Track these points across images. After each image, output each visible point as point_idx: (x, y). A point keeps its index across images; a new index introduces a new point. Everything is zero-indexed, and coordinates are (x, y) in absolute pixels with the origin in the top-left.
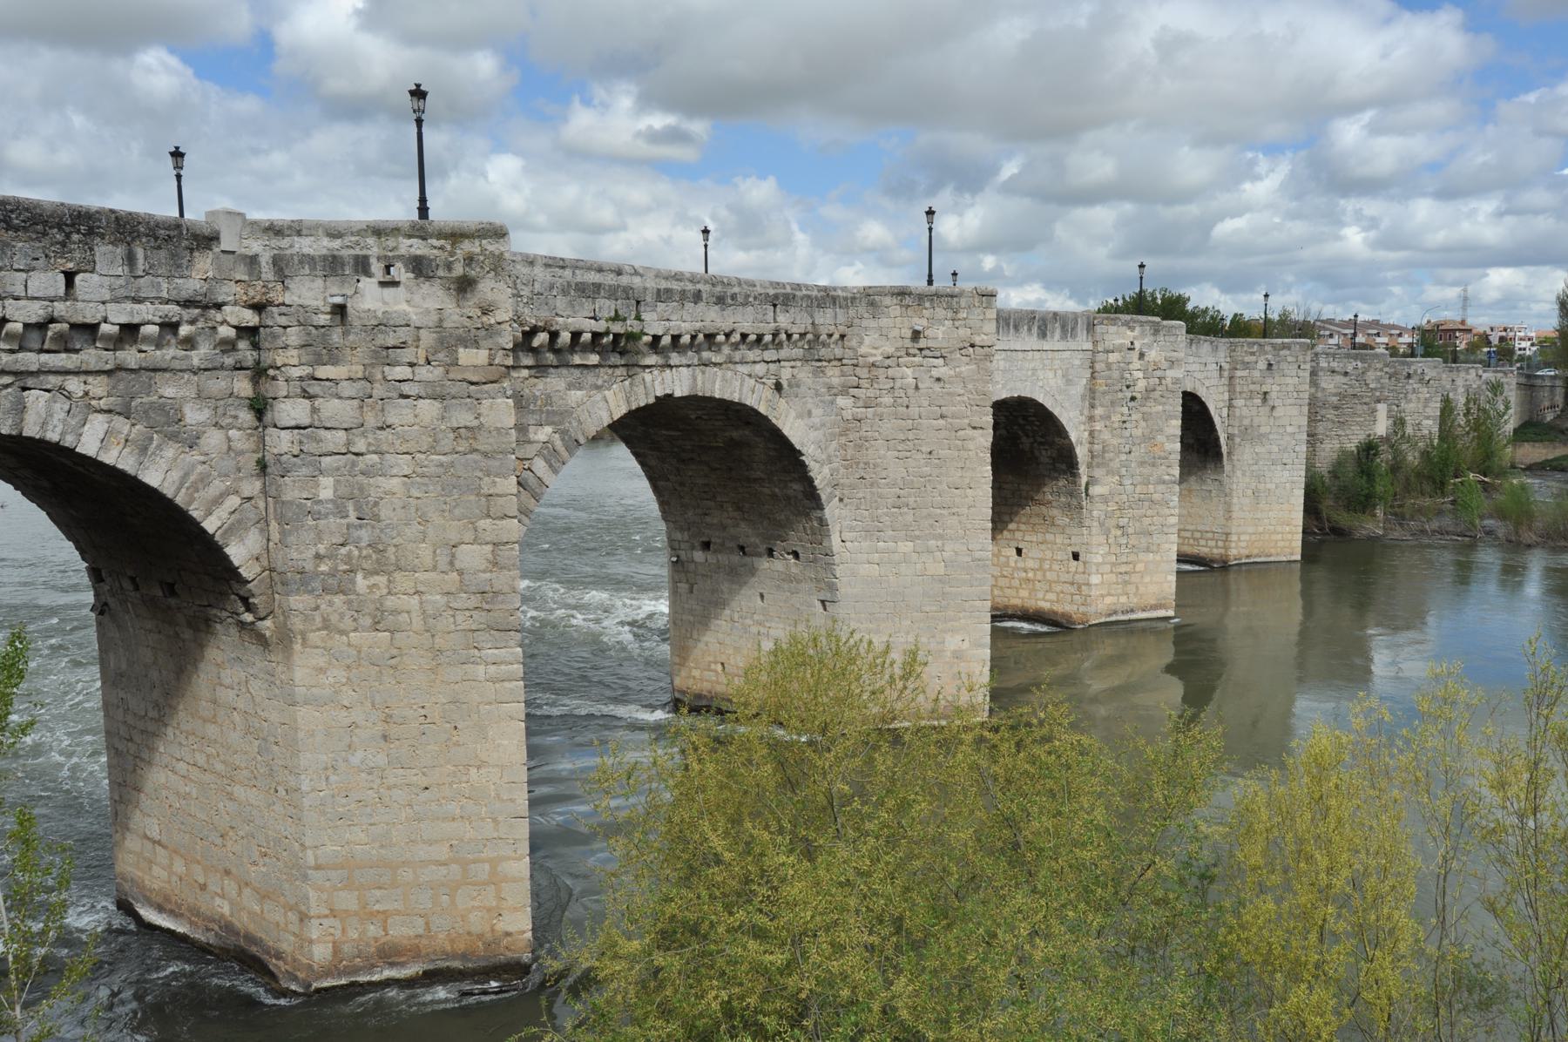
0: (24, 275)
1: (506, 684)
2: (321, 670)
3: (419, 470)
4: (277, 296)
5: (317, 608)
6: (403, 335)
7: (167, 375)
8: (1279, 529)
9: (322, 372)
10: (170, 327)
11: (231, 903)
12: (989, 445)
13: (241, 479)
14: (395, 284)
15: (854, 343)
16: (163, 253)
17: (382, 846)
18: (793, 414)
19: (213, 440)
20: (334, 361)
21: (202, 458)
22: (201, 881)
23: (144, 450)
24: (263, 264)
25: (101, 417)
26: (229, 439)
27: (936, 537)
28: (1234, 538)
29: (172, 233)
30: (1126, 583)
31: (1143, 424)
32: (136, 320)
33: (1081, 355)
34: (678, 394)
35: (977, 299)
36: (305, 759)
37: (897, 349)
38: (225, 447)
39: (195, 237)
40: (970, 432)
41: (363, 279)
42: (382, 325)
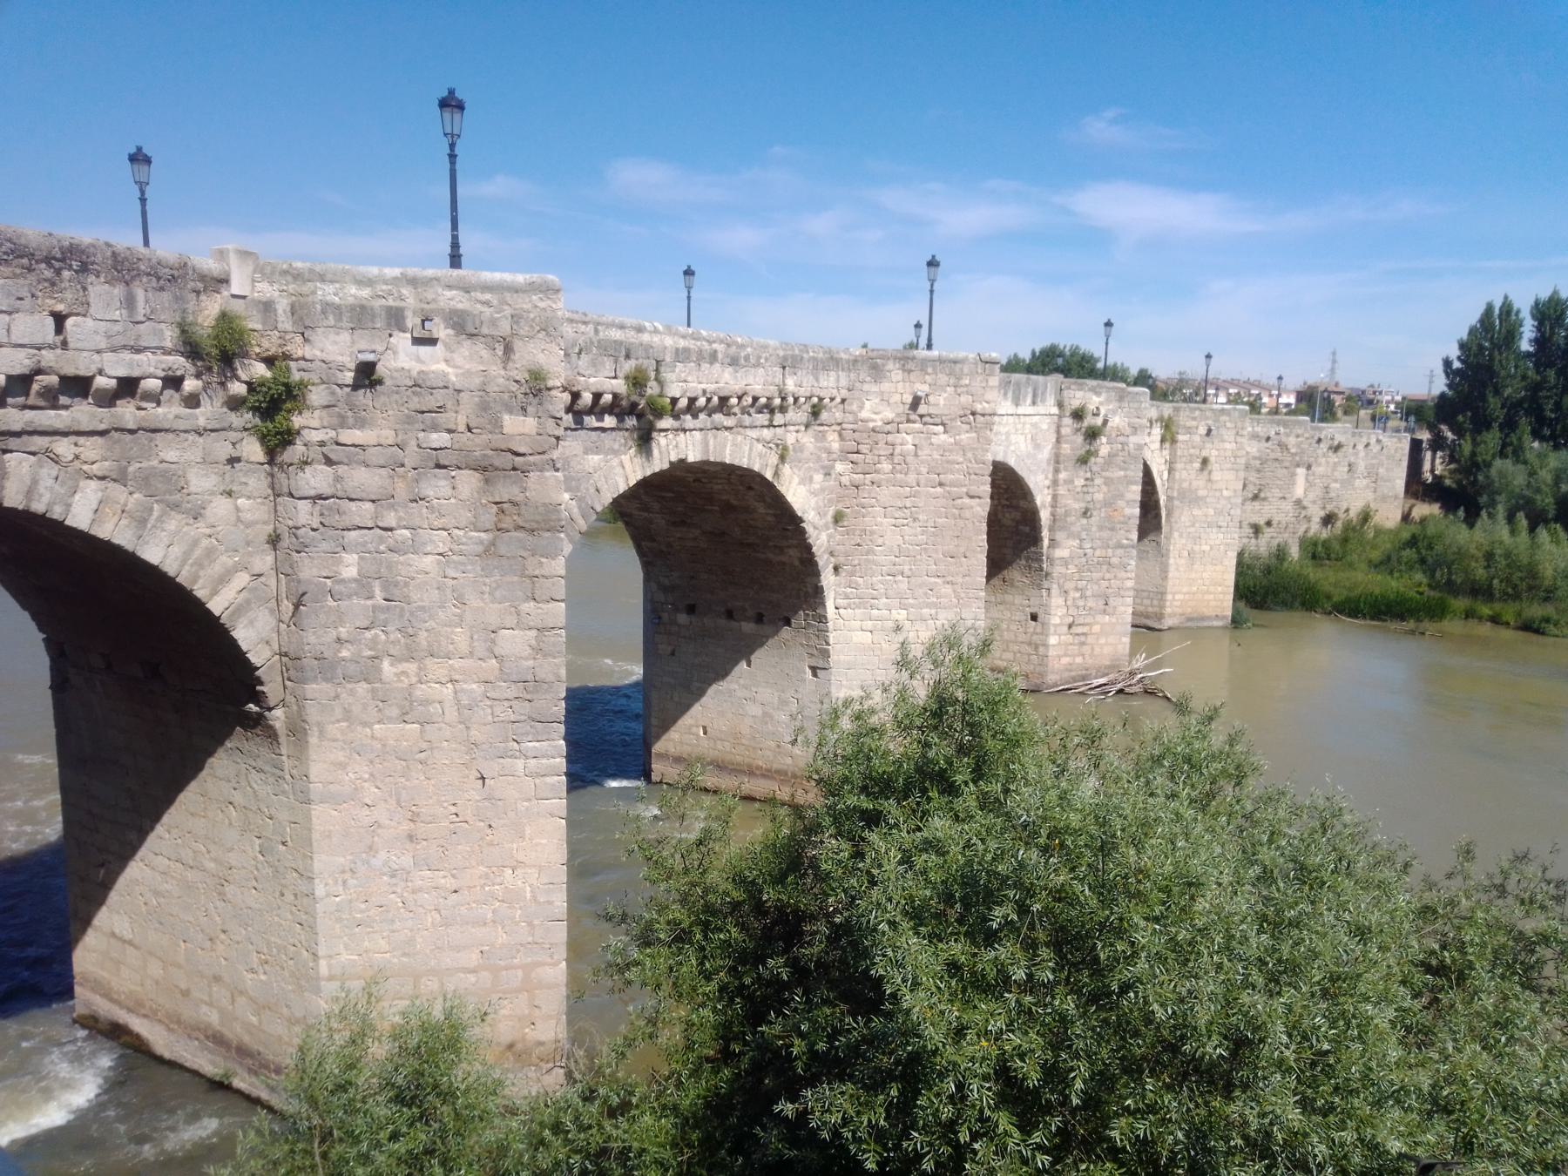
0: (7, 318)
1: (548, 780)
2: (342, 766)
3: (456, 548)
4: (297, 348)
5: (337, 697)
6: (439, 398)
7: (171, 436)
8: (1212, 589)
9: (348, 436)
10: (173, 382)
11: (221, 1011)
12: (985, 514)
13: (250, 554)
14: (432, 342)
15: (855, 407)
16: (166, 296)
17: (404, 955)
18: (796, 480)
19: (220, 508)
20: (361, 424)
21: (208, 531)
22: (183, 986)
23: (142, 522)
24: (280, 311)
25: (94, 484)
26: (238, 509)
27: (928, 606)
28: (1169, 597)
29: (176, 273)
30: (1083, 644)
31: (1105, 489)
32: (136, 373)
33: (1048, 419)
34: (691, 459)
35: (980, 365)
36: (320, 862)
37: (898, 415)
38: (233, 519)
39: (203, 278)
40: (967, 500)
41: (395, 333)
42: (418, 385)
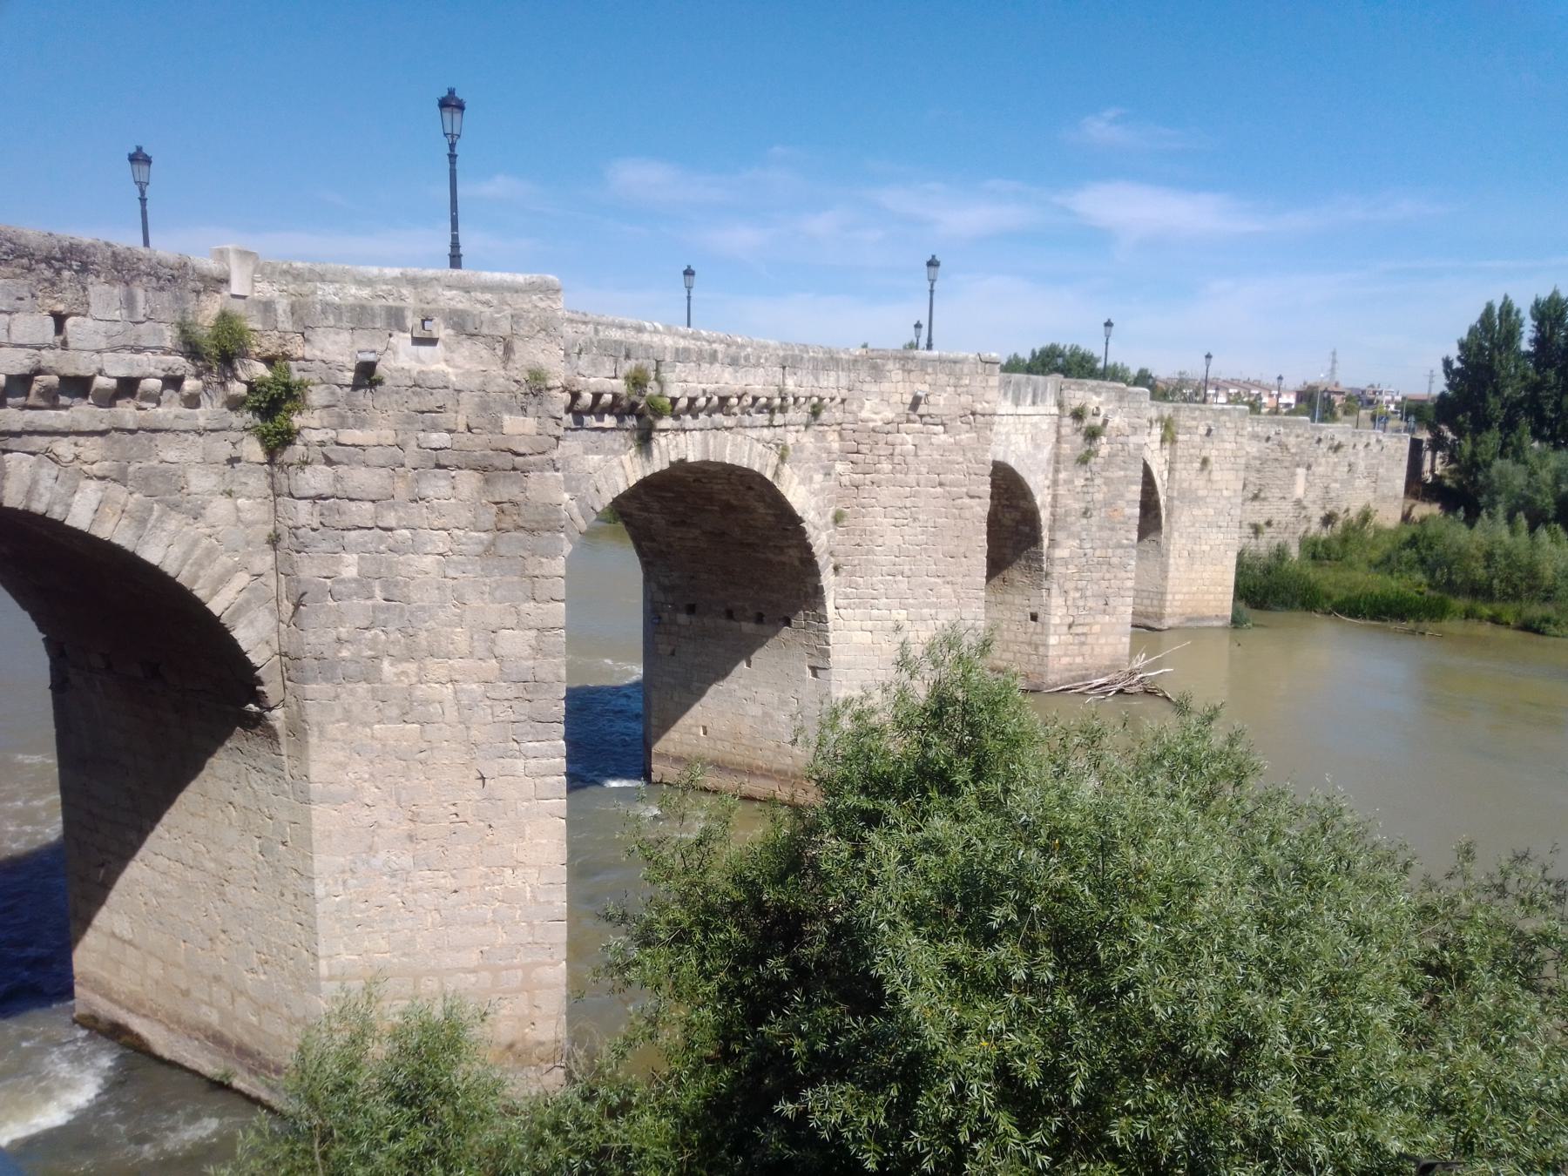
0: (7, 318)
1: (548, 780)
2: (342, 766)
3: (456, 548)
4: (297, 348)
5: (337, 697)
6: (439, 398)
7: (171, 436)
8: (1212, 589)
9: (348, 436)
10: (173, 382)
11: (221, 1011)
12: (985, 514)
13: (250, 554)
14: (432, 342)
15: (855, 407)
16: (166, 296)
17: (404, 955)
18: (796, 480)
19: (220, 508)
20: (361, 424)
21: (208, 531)
22: (183, 986)
23: (142, 522)
24: (280, 311)
25: (94, 484)
26: (238, 509)
27: (928, 606)
28: (1169, 597)
29: (176, 273)
30: (1083, 644)
31: (1105, 489)
32: (136, 373)
33: (1048, 419)
34: (691, 459)
35: (980, 365)
36: (320, 862)
37: (898, 415)
38: (233, 519)
39: (203, 278)
40: (967, 500)
41: (395, 333)
42: (418, 385)
